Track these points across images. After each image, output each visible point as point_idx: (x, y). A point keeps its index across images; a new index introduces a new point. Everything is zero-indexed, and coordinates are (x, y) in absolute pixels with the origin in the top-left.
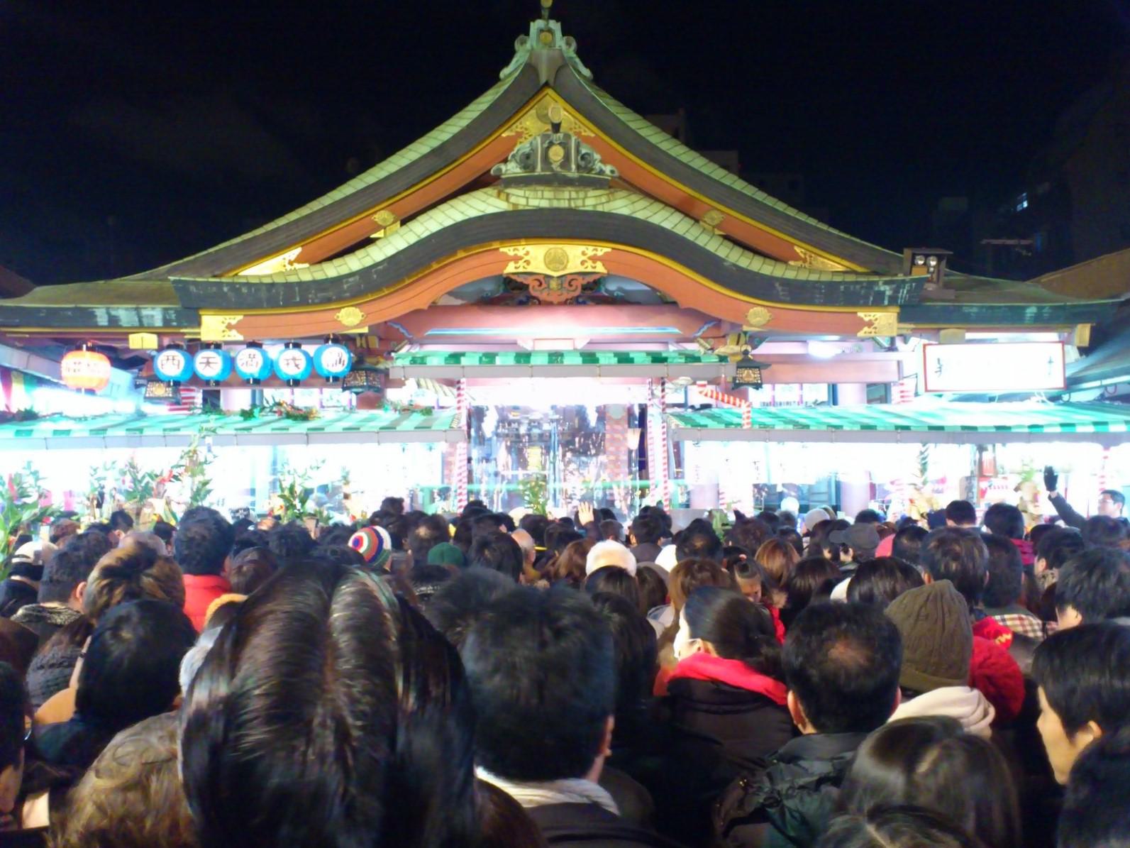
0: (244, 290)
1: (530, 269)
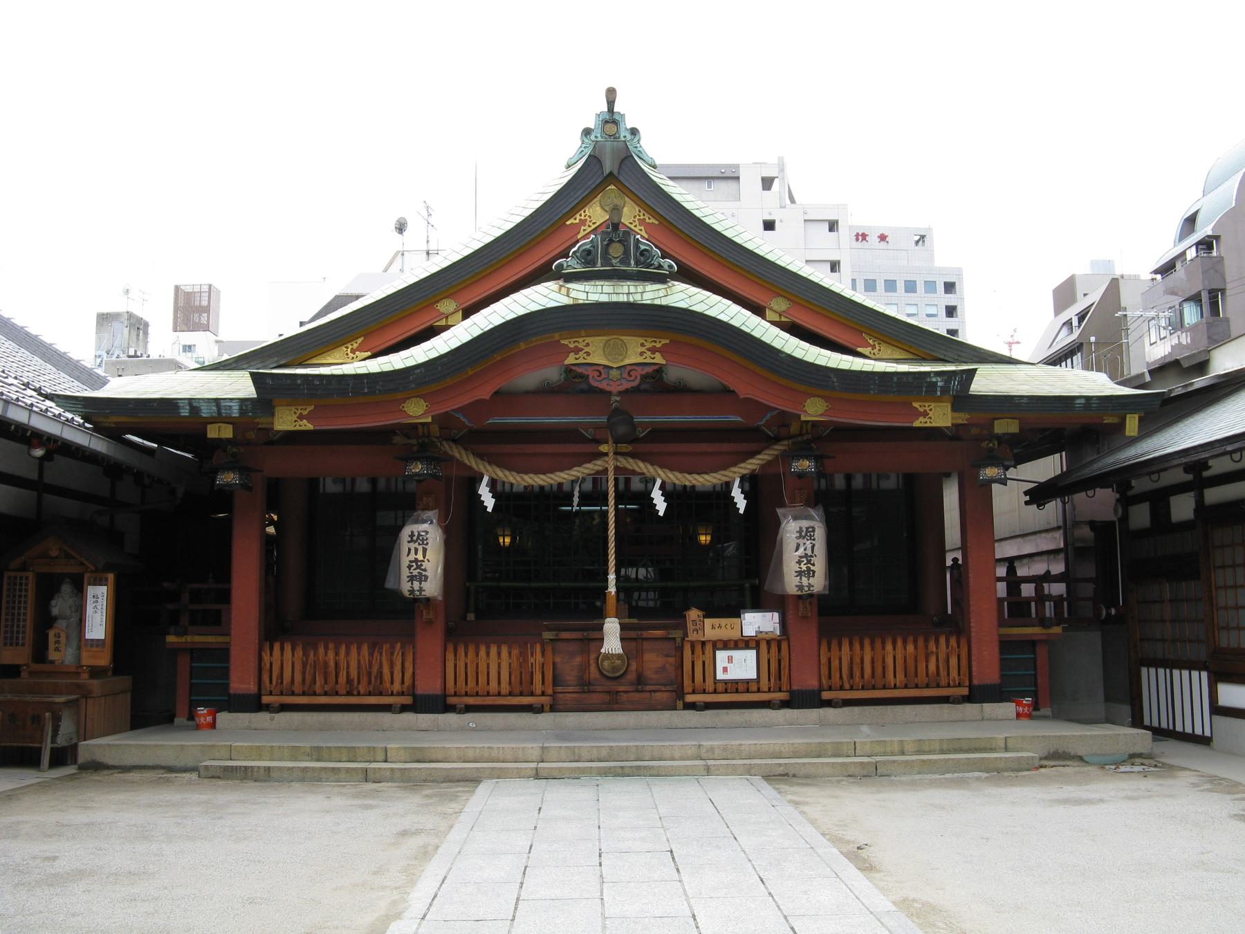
1: (589, 360)
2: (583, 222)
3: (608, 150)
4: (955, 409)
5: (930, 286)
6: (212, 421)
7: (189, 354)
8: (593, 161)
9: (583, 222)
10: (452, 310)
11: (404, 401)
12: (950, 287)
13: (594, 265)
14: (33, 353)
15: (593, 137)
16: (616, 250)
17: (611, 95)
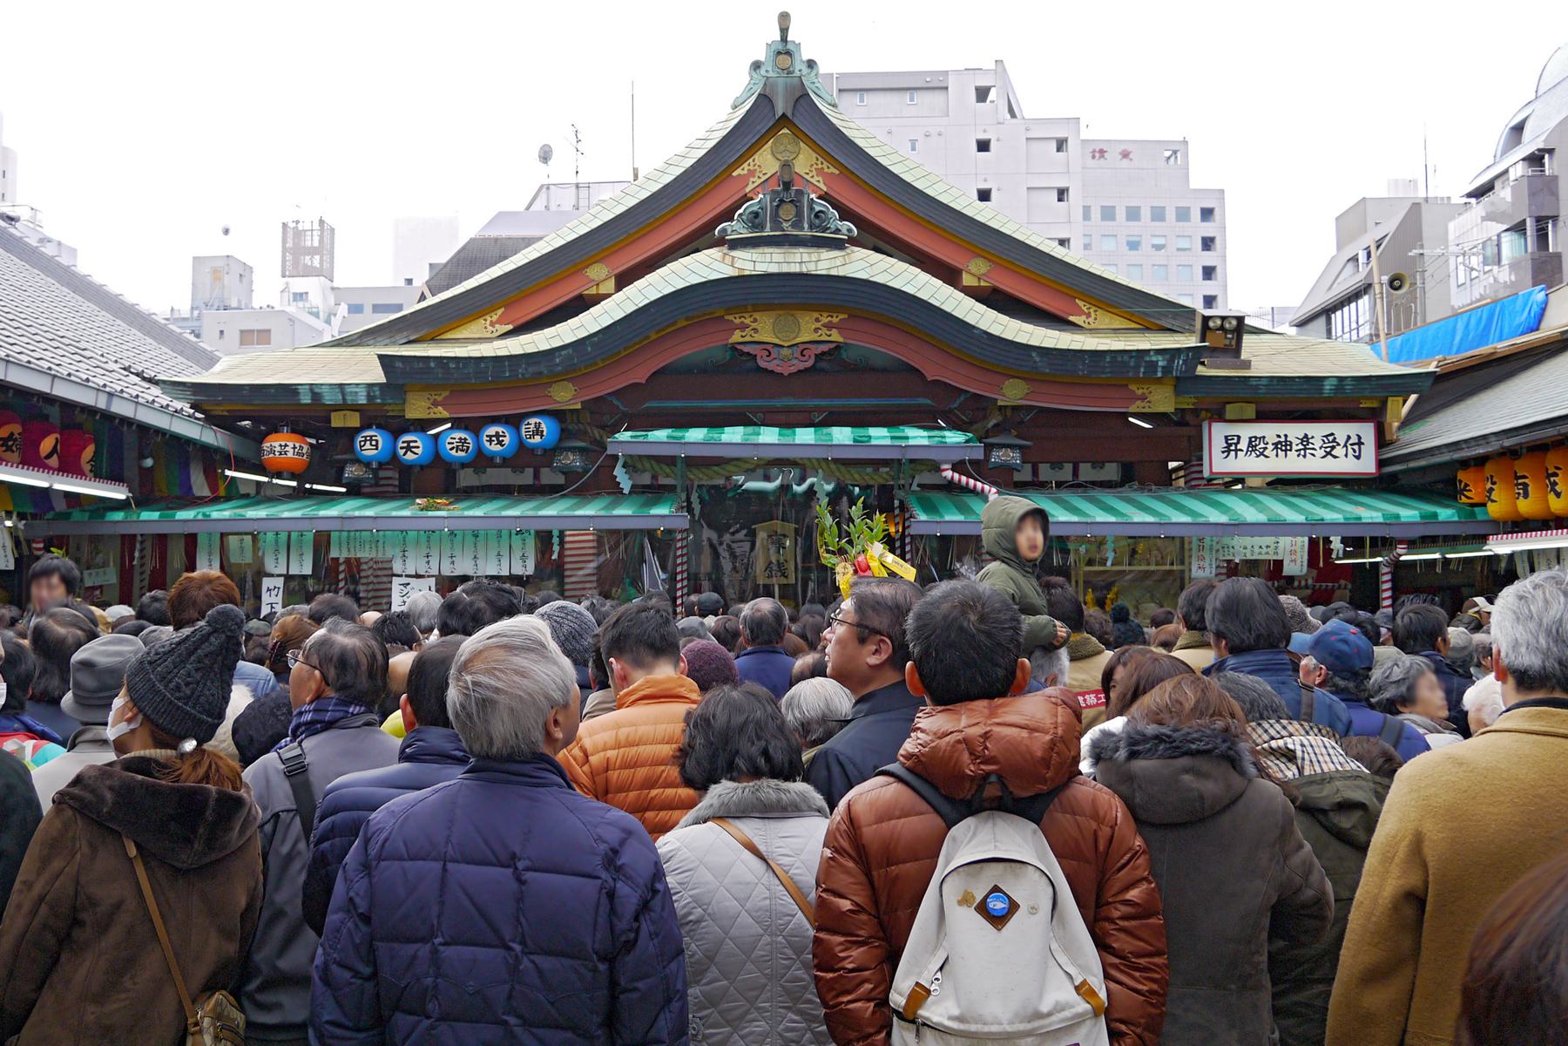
0: (452, 365)
1: (757, 338)
2: (752, 173)
3: (780, 89)
4: (1178, 392)
5: (1183, 214)
6: (336, 408)
7: (301, 304)
8: (764, 100)
9: (752, 173)
10: (603, 276)
11: (550, 384)
12: (1207, 214)
13: (762, 227)
14: (131, 324)
15: (763, 71)
16: (788, 212)
17: (784, 18)
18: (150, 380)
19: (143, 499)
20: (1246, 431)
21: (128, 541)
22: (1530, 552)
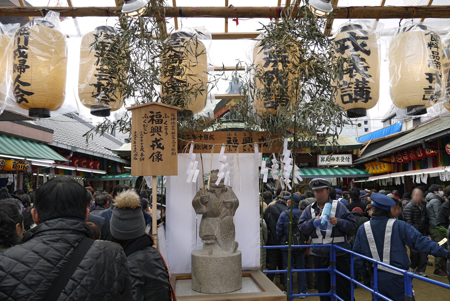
13: (228, 119)
16: (233, 116)
18: (110, 150)
19: (109, 173)
20: (326, 157)
21: (105, 182)
22: (385, 179)
